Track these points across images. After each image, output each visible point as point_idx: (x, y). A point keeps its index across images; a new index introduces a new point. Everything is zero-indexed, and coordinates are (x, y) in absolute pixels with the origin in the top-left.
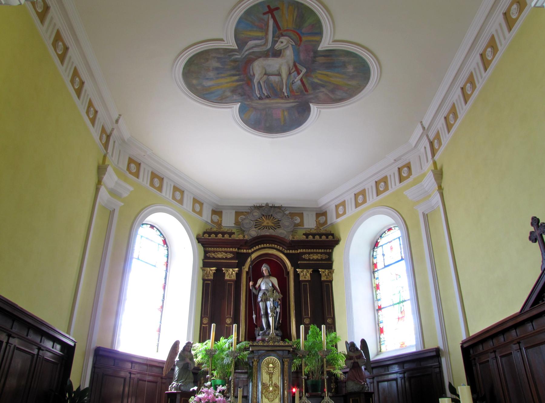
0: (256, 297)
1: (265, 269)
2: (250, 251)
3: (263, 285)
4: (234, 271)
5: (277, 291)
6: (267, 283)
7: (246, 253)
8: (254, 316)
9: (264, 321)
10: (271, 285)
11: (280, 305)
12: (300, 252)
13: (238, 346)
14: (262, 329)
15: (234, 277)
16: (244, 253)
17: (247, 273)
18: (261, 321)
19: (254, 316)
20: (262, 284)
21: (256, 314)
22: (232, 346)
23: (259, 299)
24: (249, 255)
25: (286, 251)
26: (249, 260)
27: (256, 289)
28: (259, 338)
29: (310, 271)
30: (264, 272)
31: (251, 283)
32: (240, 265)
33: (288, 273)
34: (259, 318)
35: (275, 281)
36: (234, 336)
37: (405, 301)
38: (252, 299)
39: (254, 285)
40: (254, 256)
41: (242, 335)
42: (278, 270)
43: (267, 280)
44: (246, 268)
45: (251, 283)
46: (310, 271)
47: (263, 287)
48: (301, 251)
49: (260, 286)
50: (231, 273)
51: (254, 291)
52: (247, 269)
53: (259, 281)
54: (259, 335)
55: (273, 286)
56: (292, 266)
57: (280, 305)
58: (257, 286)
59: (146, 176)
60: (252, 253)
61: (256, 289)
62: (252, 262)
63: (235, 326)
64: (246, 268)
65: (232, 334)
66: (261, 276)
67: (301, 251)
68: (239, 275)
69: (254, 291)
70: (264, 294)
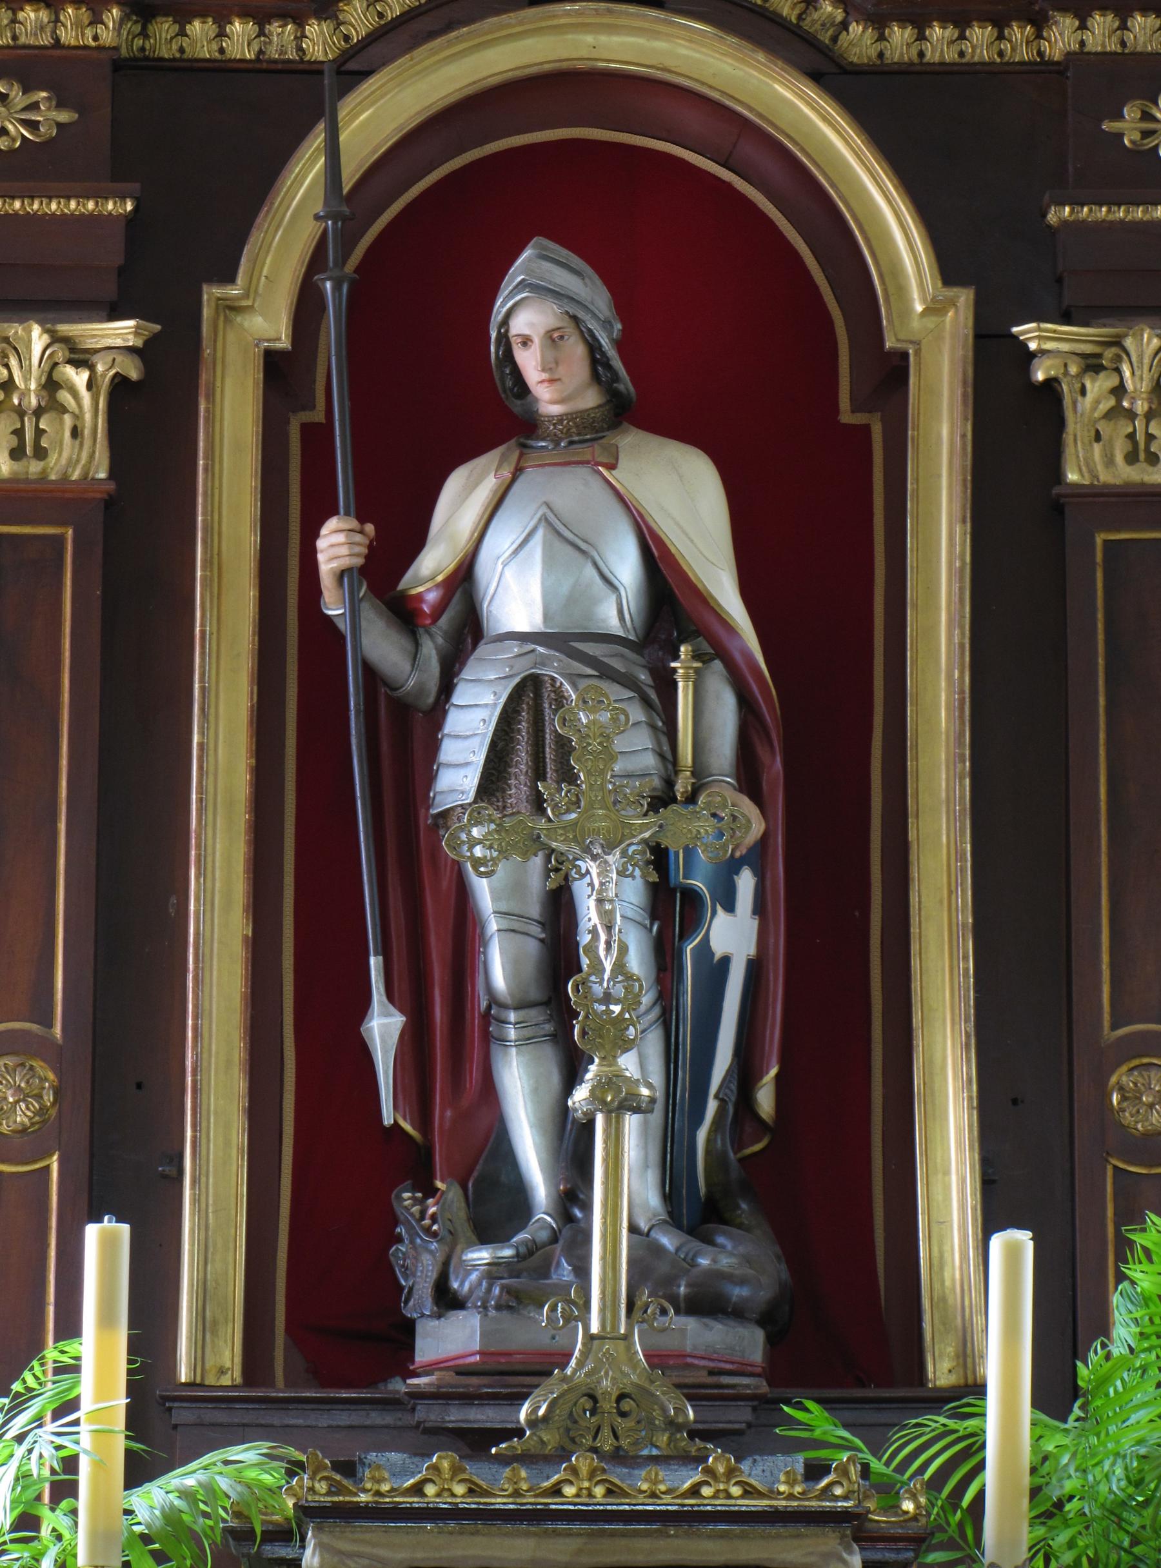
0: (411, 730)
1: (542, 322)
2: (318, 41)
3: (522, 557)
4: (81, 358)
5: (716, 645)
6: (569, 541)
7: (261, 70)
8: (383, 1027)
9: (520, 1084)
10: (626, 566)
11: (758, 858)
12: (1079, 58)
13: (151, 1501)
14: (496, 1203)
15: (78, 452)
16: (223, 69)
17: (281, 373)
18: (490, 1092)
19: (383, 1027)
20: (501, 541)
21: (412, 999)
22: (64, 1490)
23: (459, 771)
24: (304, 97)
25: (859, 41)
26: (304, 179)
27: (405, 614)
28: (448, 1340)
29: (324, 421)
30: (529, 362)
31: (337, 544)
32: (166, 269)
33: (891, 375)
34: (449, 1045)
35: (687, 497)
36: (97, 1358)
37: (516, 552)
38: (346, 748)
39: (384, 568)
40: (373, 118)
41: (203, 1291)
42: (743, 345)
43: (571, 489)
44: (257, 310)
45: (337, 544)
46: (324, 421)
47: (517, 598)
48: (1100, 33)
49: (463, 578)
50: (29, 386)
51: (380, 644)
52: (270, 324)
53: (462, 501)
54: (447, 1300)
55: (669, 597)
56: (950, 271)
57: (758, 858)
58: (433, 563)
59: (208, 934)
60: (353, 68)
61: (405, 614)
62: (348, 205)
63: (104, 1244)
64: (257, 310)
65: (69, 1328)
66: (489, 416)
67: (1100, 33)
68: (153, 414)
69: (380, 644)
70: (528, 699)
